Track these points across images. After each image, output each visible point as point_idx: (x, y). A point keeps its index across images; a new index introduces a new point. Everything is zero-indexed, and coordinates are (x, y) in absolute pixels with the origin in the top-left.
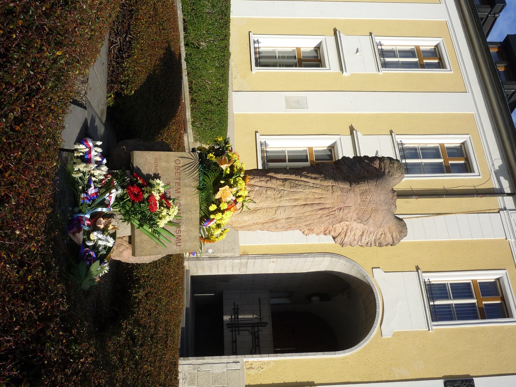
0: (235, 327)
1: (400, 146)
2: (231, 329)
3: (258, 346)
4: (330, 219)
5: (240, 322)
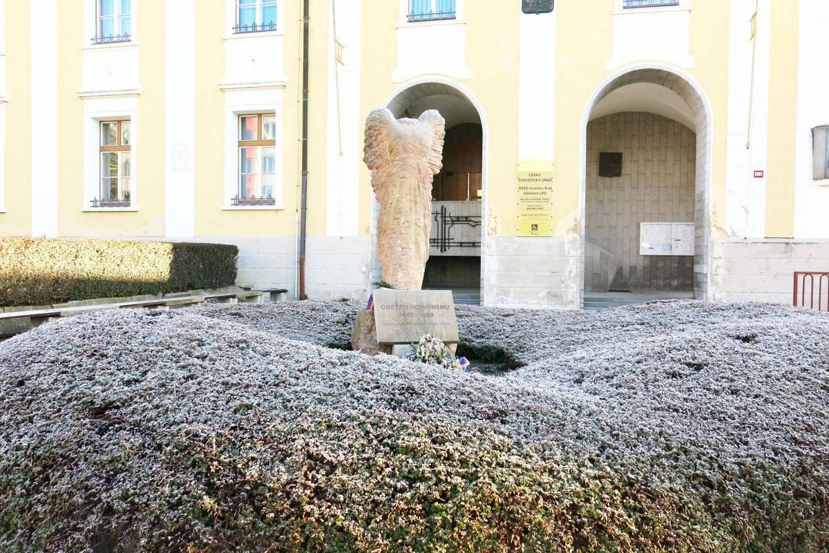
0: (445, 243)
2: (447, 248)
3: (467, 217)
5: (440, 237)
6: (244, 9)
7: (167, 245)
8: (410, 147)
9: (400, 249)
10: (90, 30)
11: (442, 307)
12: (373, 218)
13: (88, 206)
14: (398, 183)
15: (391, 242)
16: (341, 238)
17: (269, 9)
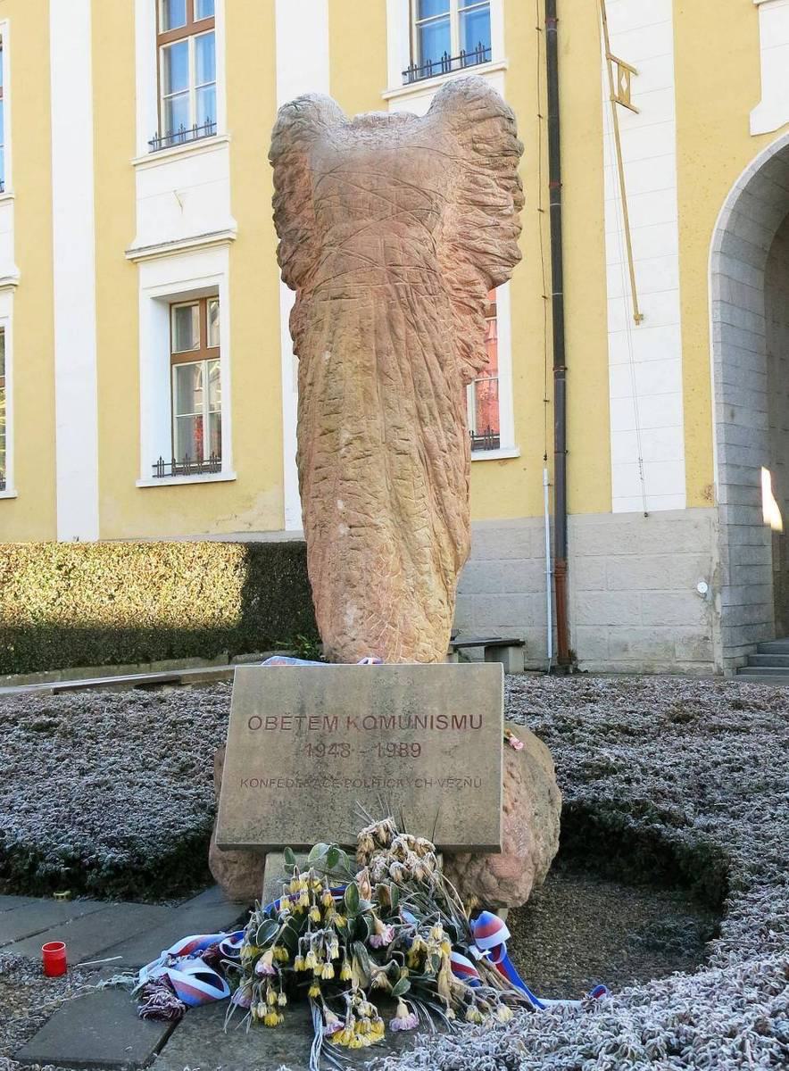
1: (416, 74)
4: (421, 302)
6: (431, 30)
7: (233, 549)
8: (363, 194)
9: (343, 530)
10: (147, 123)
11: (458, 723)
12: (720, 465)
13: (147, 477)
14: (328, 319)
15: (319, 507)
16: (646, 515)
17: (477, 21)
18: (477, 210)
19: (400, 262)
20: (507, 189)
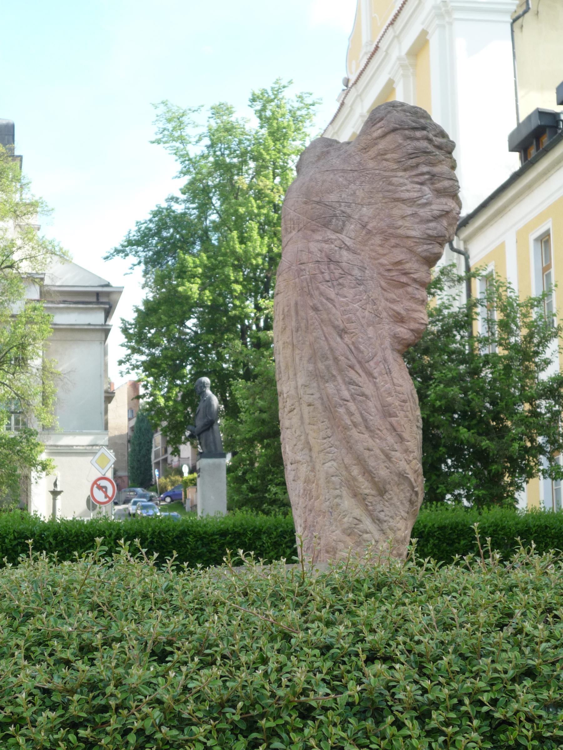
18: (400, 205)
19: (305, 261)
20: (422, 184)
